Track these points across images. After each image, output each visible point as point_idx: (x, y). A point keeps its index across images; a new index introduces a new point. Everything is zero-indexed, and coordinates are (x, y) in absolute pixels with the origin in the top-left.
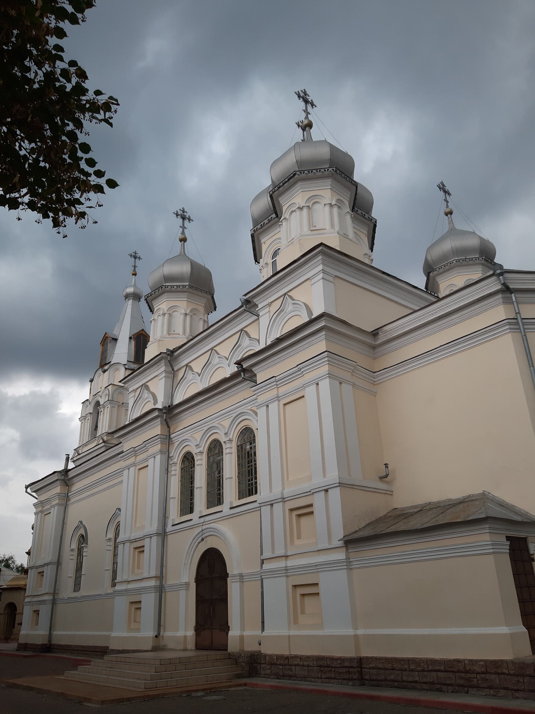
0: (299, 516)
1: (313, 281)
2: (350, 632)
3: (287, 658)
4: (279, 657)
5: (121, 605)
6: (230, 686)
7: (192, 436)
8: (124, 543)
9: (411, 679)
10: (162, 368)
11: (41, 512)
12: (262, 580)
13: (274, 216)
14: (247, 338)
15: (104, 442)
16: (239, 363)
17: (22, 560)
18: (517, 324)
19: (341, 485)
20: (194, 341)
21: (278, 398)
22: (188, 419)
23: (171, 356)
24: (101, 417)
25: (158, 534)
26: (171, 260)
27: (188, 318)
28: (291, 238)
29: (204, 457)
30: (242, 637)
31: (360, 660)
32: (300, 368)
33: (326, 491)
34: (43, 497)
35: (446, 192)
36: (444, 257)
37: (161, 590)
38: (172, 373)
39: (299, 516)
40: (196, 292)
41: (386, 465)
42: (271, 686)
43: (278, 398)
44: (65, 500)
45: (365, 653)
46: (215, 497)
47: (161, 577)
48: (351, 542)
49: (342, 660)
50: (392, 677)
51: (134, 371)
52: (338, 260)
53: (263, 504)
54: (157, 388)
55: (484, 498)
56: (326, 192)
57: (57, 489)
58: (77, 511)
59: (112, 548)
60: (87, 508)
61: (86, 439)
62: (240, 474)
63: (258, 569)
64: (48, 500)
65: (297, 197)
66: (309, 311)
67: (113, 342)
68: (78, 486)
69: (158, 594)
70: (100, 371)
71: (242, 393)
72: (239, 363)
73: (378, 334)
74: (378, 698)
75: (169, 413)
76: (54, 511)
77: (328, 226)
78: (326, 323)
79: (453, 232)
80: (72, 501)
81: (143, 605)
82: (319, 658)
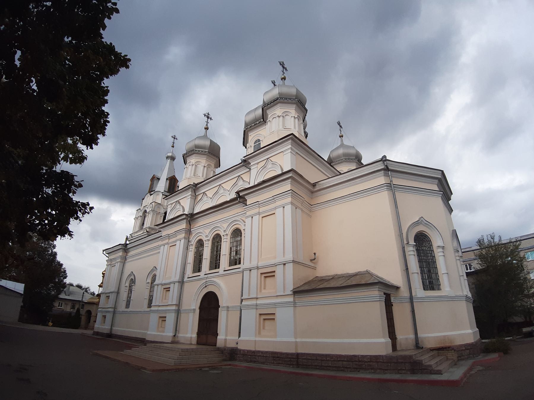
0: (266, 277)
1: (285, 153)
2: (293, 340)
3: (254, 352)
4: (248, 351)
5: (154, 319)
6: (222, 366)
7: (204, 230)
8: (158, 285)
9: (326, 365)
10: (189, 193)
11: (110, 265)
12: (241, 310)
13: (262, 120)
14: (242, 181)
15: (147, 232)
16: (238, 193)
17: (96, 290)
18: (390, 186)
19: (293, 261)
20: (207, 181)
21: (259, 213)
22: (201, 222)
23: (195, 187)
24: (146, 218)
25: (179, 282)
26: (199, 138)
27: (206, 168)
28: (266, 134)
29: (210, 243)
30: (226, 340)
31: (298, 355)
32: (274, 198)
33: (284, 264)
34: (110, 258)
35: (341, 126)
36: (339, 157)
37: (178, 312)
38: (195, 197)
39: (266, 277)
40: (211, 156)
41: (315, 254)
42: (246, 367)
43: (259, 213)
44: (124, 260)
45: (300, 351)
46: (215, 264)
47: (179, 305)
48: (297, 292)
49: (287, 354)
50: (316, 364)
51: (167, 196)
52: (299, 145)
53: (246, 269)
54: (185, 203)
55: (368, 273)
56: (293, 110)
57: (120, 254)
58: (130, 267)
59: (149, 288)
60: (138, 265)
61: (137, 230)
62: (211, 257)
63: (239, 304)
64: (115, 259)
65: (278, 110)
66: (282, 169)
67: (157, 180)
68: (132, 253)
69: (176, 314)
70: (149, 194)
71: (236, 210)
72: (238, 193)
73: (316, 185)
74: (312, 375)
75: (191, 218)
76: (118, 265)
77: (201, 176)
78: (293, 175)
79: (342, 145)
80: (128, 261)
81: (167, 319)
82: (273, 353)
